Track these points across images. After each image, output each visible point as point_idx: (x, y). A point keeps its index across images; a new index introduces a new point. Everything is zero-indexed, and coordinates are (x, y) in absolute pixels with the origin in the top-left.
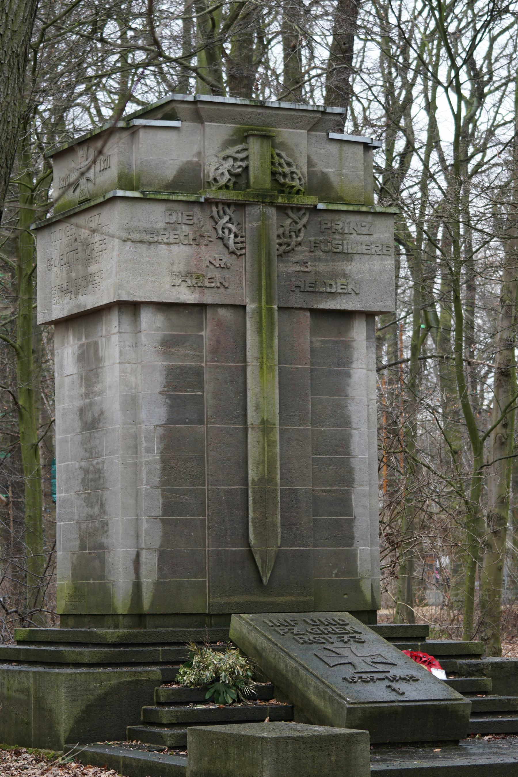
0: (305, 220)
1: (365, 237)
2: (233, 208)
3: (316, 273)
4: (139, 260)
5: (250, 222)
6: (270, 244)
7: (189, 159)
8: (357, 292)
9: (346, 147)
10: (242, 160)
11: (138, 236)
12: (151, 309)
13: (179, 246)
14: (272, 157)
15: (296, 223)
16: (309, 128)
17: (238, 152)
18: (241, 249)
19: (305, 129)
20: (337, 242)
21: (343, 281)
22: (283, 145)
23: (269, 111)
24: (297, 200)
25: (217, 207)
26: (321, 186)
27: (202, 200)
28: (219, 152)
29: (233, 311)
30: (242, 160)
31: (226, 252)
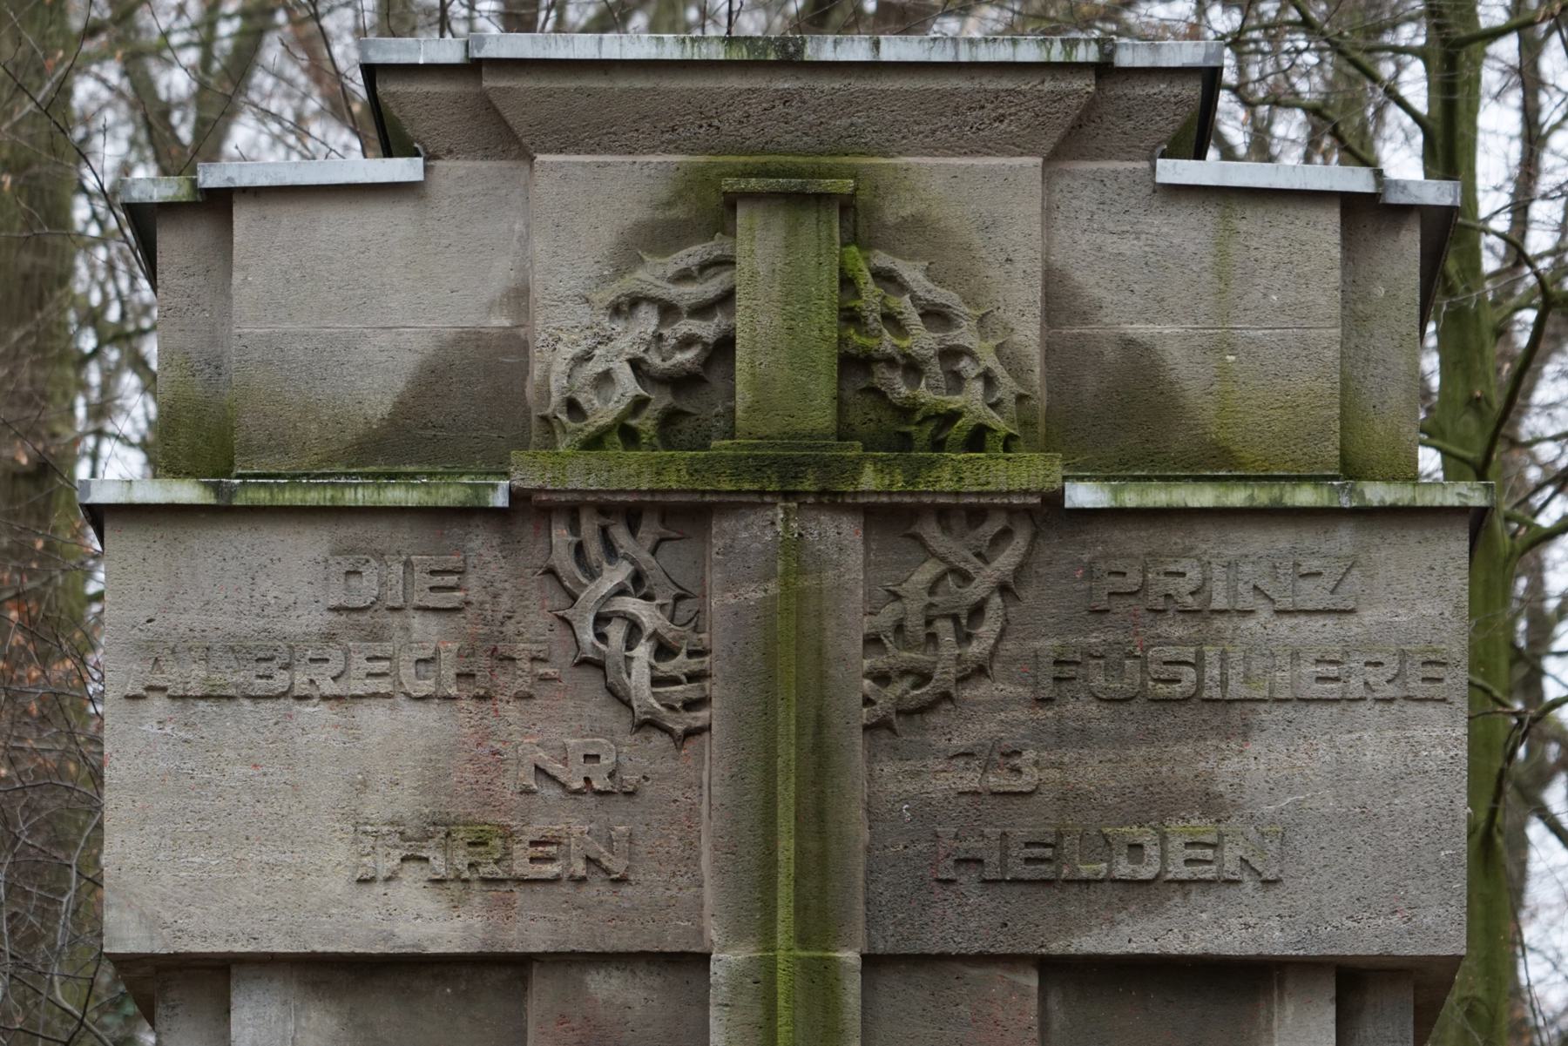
0: (1006, 560)
1: (1317, 623)
2: (650, 530)
3: (1063, 798)
4: (202, 776)
5: (730, 584)
6: (822, 676)
7: (471, 320)
8: (1267, 876)
9: (1250, 221)
10: (702, 310)
11: (199, 671)
12: (276, 984)
13: (393, 708)
14: (847, 282)
15: (965, 578)
16: (1048, 144)
17: (684, 277)
18: (690, 705)
19: (1032, 153)
20: (1170, 653)
21: (1203, 827)
22: (919, 232)
23: (826, 84)
24: (952, 475)
25: (574, 528)
26: (1120, 408)
27: (500, 499)
28: (603, 280)
29: (656, 982)
30: (702, 310)
31: (611, 716)
